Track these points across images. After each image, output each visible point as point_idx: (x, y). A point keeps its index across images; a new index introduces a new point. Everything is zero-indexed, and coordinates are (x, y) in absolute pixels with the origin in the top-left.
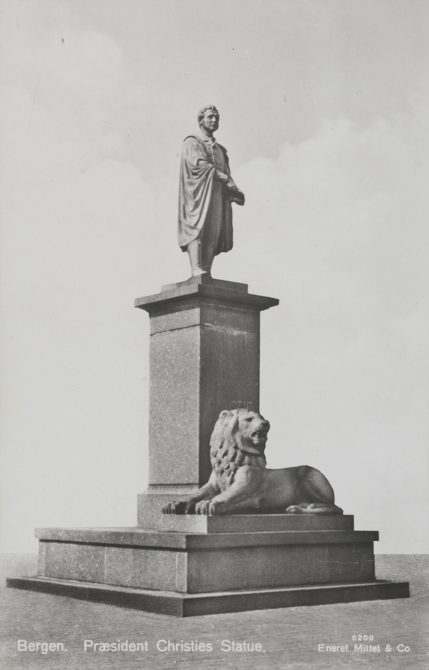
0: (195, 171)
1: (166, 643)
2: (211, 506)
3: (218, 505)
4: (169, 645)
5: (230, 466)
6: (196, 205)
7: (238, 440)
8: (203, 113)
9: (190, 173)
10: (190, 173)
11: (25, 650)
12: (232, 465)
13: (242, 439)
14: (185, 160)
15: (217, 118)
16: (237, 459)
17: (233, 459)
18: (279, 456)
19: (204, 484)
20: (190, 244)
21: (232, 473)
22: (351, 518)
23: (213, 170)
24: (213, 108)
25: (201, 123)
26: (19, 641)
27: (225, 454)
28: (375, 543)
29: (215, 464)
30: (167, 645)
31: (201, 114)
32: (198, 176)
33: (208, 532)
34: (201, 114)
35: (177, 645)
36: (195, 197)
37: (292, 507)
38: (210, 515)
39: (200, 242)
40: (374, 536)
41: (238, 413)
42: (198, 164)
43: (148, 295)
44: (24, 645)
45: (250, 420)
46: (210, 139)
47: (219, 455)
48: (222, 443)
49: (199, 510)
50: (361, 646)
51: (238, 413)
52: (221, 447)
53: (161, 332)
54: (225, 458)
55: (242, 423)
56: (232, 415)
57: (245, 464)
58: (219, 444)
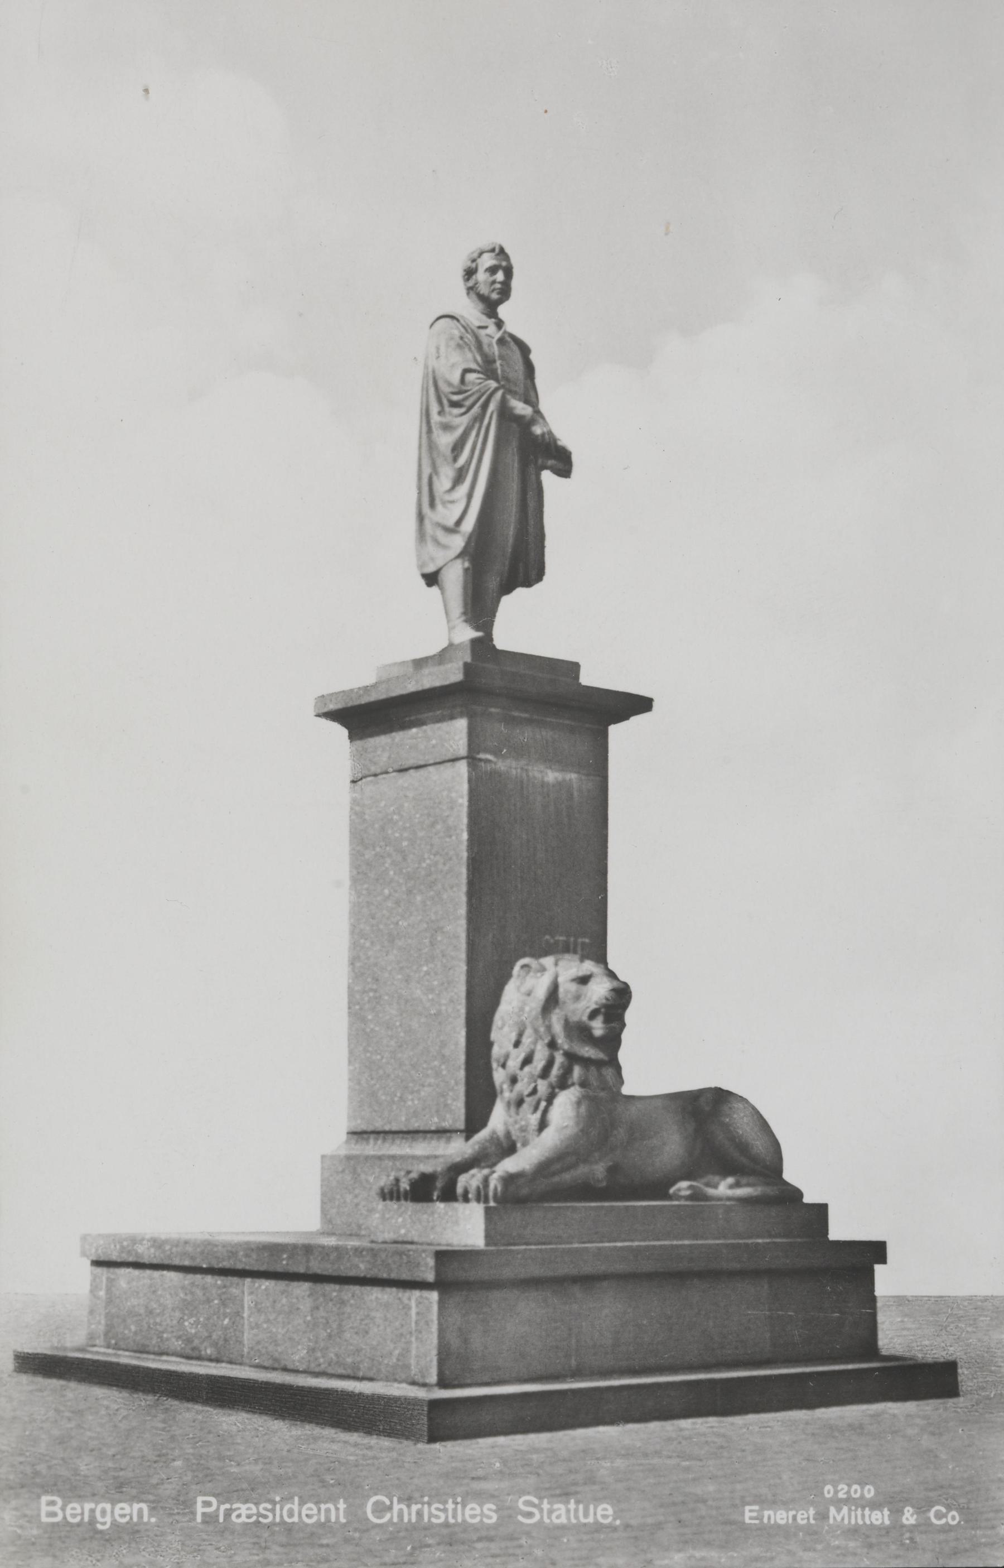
0: (455, 398)
1: (388, 1502)
2: (494, 1182)
4: (396, 1507)
5: (539, 1088)
6: (458, 479)
7: (558, 1028)
8: (474, 261)
9: (445, 402)
10: (445, 402)
11: (59, 1518)
12: (543, 1086)
13: (567, 1025)
14: (434, 372)
15: (509, 272)
16: (555, 1071)
17: (545, 1073)
18: (652, 1066)
19: (476, 1131)
21: (543, 1104)
23: (499, 395)
24: (497, 250)
25: (471, 284)
26: (44, 1499)
27: (528, 1060)
28: (878, 1268)
30: (390, 1508)
31: (469, 264)
32: (463, 410)
34: (469, 264)
36: (455, 459)
37: (684, 1184)
41: (556, 964)
42: (462, 381)
44: (56, 1508)
46: (491, 323)
47: (513, 1064)
50: (845, 1510)
51: (556, 964)
52: (517, 1044)
53: (375, 775)
54: (527, 1069)
55: (567, 988)
56: (543, 969)
57: (573, 1084)
58: (513, 1037)
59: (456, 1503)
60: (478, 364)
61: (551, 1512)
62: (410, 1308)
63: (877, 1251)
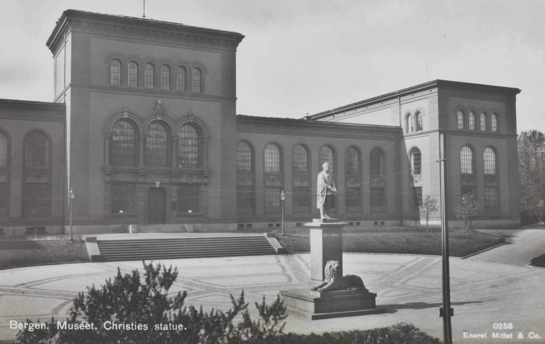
1: (110, 323)
3: (324, 289)
4: (113, 325)
11: (16, 328)
18: (346, 272)
22: (57, 22)
26: (11, 321)
30: (111, 325)
35: (120, 325)
43: (311, 240)
44: (16, 324)
50: (497, 334)
55: (332, 265)
59: (134, 323)
61: (163, 327)
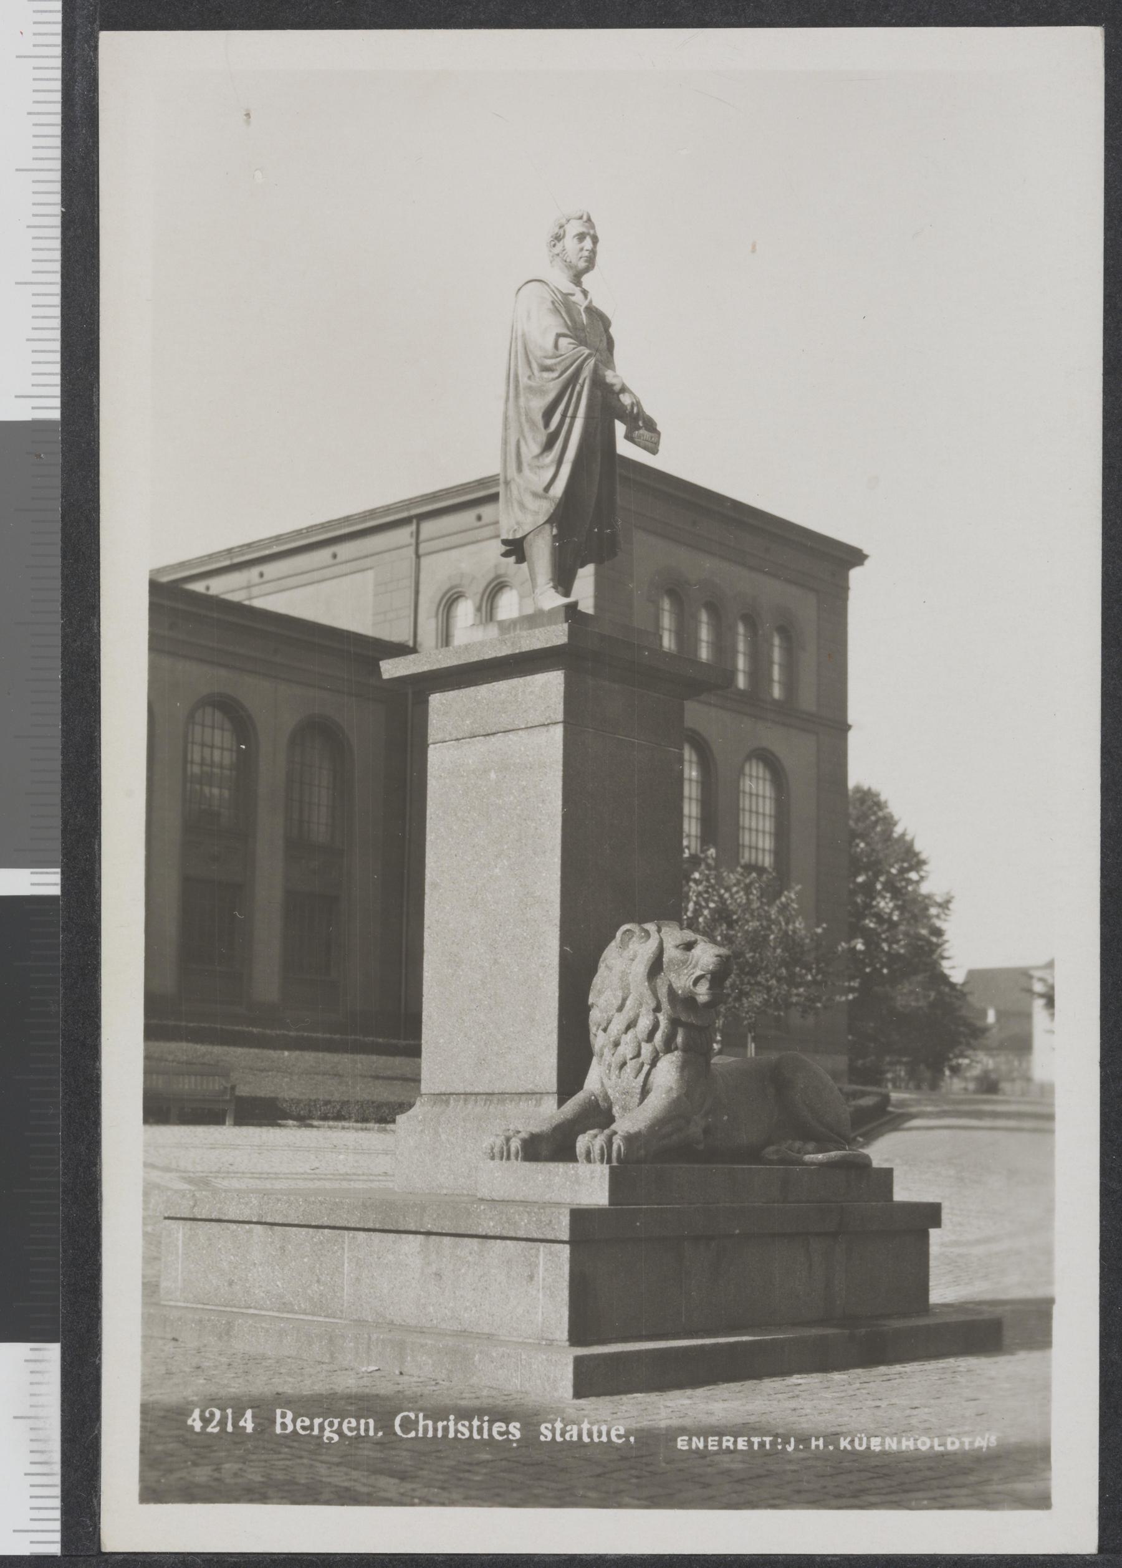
0: (549, 362)
2: (617, 1142)
5: (643, 1051)
6: (549, 445)
7: (663, 992)
8: (561, 227)
9: (535, 366)
10: (535, 366)
12: (647, 1050)
13: (671, 991)
14: (523, 335)
15: (595, 240)
16: (659, 1036)
17: (650, 1037)
19: (571, 1094)
20: (529, 537)
21: (646, 1068)
23: (591, 362)
24: (585, 218)
25: (557, 250)
27: (631, 1025)
28: (933, 1232)
29: (604, 1046)
31: (556, 230)
32: (556, 374)
33: (610, 1204)
34: (556, 230)
36: (547, 425)
37: (771, 1148)
38: (615, 1164)
39: (555, 531)
40: (931, 1214)
41: (659, 931)
42: (556, 346)
45: (689, 946)
46: (577, 290)
47: (616, 1027)
48: (624, 1000)
49: (588, 1153)
51: (659, 931)
52: (620, 1009)
53: (457, 740)
54: (631, 1033)
55: (671, 953)
56: (648, 934)
57: (676, 1049)
58: (617, 1003)
60: (568, 328)
62: (537, 1266)
63: (931, 1214)
